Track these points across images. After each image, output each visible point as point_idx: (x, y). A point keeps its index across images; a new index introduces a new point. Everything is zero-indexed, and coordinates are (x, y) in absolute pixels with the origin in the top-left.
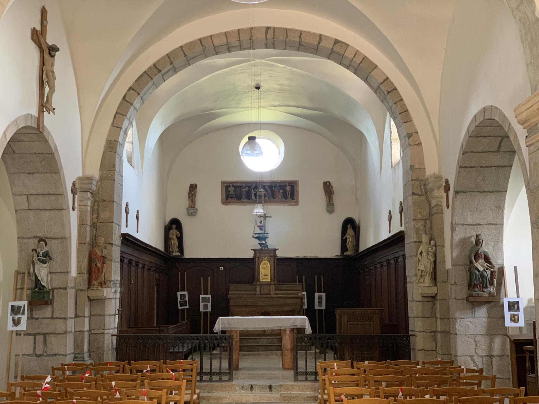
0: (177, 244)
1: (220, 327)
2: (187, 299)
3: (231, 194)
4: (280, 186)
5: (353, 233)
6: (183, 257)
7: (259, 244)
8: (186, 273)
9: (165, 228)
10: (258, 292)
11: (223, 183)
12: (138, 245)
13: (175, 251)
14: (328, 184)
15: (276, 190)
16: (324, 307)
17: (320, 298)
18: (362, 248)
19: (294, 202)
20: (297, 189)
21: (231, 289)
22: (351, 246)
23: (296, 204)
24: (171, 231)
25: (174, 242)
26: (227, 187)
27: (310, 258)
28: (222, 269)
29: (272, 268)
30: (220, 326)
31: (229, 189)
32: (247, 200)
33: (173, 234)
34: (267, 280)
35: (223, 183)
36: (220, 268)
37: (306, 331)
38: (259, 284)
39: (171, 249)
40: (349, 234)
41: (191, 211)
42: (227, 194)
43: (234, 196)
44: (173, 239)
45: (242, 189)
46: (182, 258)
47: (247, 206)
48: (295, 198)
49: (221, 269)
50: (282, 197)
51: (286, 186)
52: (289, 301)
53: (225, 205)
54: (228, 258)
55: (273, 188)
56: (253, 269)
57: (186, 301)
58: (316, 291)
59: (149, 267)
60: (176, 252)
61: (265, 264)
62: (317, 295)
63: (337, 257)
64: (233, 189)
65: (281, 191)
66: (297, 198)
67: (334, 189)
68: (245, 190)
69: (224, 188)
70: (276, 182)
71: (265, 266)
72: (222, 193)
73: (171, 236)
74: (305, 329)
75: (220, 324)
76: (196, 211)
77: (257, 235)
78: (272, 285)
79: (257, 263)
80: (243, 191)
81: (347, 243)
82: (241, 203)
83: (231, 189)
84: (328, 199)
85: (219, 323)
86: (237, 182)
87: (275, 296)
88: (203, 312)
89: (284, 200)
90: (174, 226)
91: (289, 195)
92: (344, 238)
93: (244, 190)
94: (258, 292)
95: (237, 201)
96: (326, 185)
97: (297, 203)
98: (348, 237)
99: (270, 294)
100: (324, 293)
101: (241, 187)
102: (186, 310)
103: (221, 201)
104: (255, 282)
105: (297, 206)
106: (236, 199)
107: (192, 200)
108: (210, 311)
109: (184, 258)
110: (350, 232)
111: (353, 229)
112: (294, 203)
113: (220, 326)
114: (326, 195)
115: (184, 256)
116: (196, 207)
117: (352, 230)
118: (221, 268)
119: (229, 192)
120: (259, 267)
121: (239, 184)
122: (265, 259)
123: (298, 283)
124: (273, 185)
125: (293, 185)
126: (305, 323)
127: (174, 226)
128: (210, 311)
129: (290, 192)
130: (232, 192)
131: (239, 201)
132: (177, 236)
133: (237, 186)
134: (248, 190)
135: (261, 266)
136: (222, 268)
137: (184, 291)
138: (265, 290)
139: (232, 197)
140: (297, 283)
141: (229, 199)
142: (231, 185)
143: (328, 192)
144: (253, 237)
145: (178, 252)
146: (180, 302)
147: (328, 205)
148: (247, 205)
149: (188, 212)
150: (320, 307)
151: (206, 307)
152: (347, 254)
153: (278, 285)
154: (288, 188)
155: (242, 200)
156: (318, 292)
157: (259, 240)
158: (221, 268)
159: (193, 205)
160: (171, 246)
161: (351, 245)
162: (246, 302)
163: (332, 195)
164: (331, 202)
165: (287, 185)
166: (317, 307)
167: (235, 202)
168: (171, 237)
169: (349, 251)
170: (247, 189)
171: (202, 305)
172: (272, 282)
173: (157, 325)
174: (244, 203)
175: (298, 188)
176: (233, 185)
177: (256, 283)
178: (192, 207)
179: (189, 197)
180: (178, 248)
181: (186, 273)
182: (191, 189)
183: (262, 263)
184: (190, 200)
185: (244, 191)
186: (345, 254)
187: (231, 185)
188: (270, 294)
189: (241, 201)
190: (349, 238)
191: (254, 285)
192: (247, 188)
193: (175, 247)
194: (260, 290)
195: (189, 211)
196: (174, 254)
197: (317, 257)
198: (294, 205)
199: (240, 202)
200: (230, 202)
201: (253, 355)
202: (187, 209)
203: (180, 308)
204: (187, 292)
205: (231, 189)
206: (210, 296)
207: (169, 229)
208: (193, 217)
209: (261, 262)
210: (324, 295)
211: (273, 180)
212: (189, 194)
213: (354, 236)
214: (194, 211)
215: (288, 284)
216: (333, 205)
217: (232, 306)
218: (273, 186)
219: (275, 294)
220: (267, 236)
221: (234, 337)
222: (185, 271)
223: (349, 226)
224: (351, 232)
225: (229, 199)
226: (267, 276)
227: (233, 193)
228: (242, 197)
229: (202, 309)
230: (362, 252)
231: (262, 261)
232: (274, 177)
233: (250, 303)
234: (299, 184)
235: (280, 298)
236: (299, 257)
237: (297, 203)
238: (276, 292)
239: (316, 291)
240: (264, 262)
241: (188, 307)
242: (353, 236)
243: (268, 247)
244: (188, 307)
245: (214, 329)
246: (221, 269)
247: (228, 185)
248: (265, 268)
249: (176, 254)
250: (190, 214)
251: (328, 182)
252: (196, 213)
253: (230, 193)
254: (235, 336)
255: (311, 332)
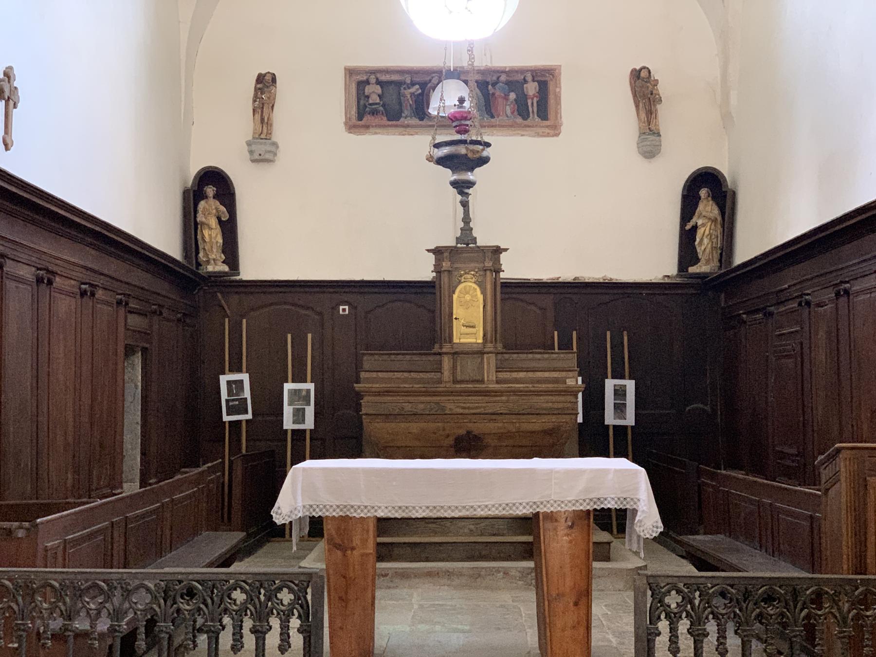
0: (221, 241)
1: (300, 504)
2: (247, 393)
3: (371, 104)
4: (508, 83)
5: (716, 212)
6: (238, 278)
7: (455, 184)
8: (244, 321)
9: (186, 193)
10: (447, 374)
11: (350, 72)
12: (78, 226)
13: (214, 260)
14: (644, 74)
15: (498, 93)
16: (630, 420)
17: (620, 393)
18: (744, 253)
19: (547, 127)
20: (558, 90)
21: (366, 366)
22: (708, 250)
23: (552, 132)
24: (202, 204)
25: (210, 235)
26: (361, 85)
27: (590, 281)
28: (347, 312)
29: (489, 308)
30: (299, 498)
31: (368, 90)
32: (415, 121)
33: (206, 213)
34: (473, 341)
35: (350, 72)
36: (341, 307)
37: (640, 521)
38: (448, 351)
39: (201, 255)
40: (704, 213)
41: (260, 148)
42: (362, 102)
43: (381, 108)
44: (208, 225)
45: (402, 91)
46: (237, 281)
47: (416, 137)
48: (551, 115)
49: (344, 310)
50: (512, 113)
51: (525, 81)
52: (542, 402)
53: (354, 133)
54: (362, 281)
55: (490, 87)
56: (433, 312)
57: (289, 405)
58: (609, 375)
59: (83, 286)
60: (216, 264)
61: (467, 293)
62: (610, 384)
63: (667, 280)
64: (378, 89)
65: (512, 96)
66: (556, 117)
67: (663, 89)
68: (412, 94)
69: (354, 86)
70: (498, 72)
71: (468, 297)
72: (347, 100)
73: (200, 218)
74: (635, 512)
75: (299, 492)
76: (273, 149)
77: (445, 151)
78: (488, 353)
79: (445, 292)
80: (404, 96)
81: (698, 240)
82: (401, 129)
83: (373, 90)
84: (643, 115)
85: (294, 483)
86: (387, 71)
87: (497, 387)
88: (293, 431)
89: (519, 120)
90: (210, 191)
91: (533, 107)
92: (688, 227)
93: (408, 92)
94: (447, 374)
95: (390, 123)
96: (638, 77)
97: (555, 130)
98: (700, 222)
99: (482, 381)
100: (630, 379)
101: (399, 84)
102: (244, 425)
103: (346, 124)
104: (437, 346)
105: (555, 138)
106: (385, 118)
107: (262, 120)
108: (313, 427)
109: (241, 281)
110: (707, 208)
111: (714, 198)
112: (547, 130)
113: (299, 498)
114: (637, 106)
115: (238, 274)
116: (275, 138)
117: (711, 202)
118: (344, 309)
119: (368, 97)
120: (451, 302)
121: (395, 78)
122: (469, 276)
123: (559, 349)
124: (489, 79)
125: (543, 79)
126: (637, 489)
127: (210, 191)
128: (313, 427)
129: (535, 100)
130: (374, 99)
131: (394, 123)
132: (219, 219)
133: (390, 83)
134: (420, 91)
135: (455, 297)
136: (347, 307)
137: (240, 371)
138: (468, 367)
139: (374, 113)
140: (557, 350)
141: (365, 119)
142: (373, 80)
143: (644, 96)
144: (430, 159)
145: (223, 262)
146: (227, 401)
147: (642, 133)
148: (417, 133)
149: (251, 152)
150: (620, 418)
151: (299, 416)
152: (698, 271)
153: (507, 356)
154: (531, 88)
155: (402, 119)
156: (613, 378)
157: (454, 169)
158: (344, 309)
159: (265, 131)
160: (201, 247)
161: (709, 246)
162: (410, 405)
163: (655, 105)
164: (652, 127)
165: (529, 77)
166: (610, 419)
167: (384, 126)
168: (204, 220)
169: (703, 261)
170: (416, 89)
171: (288, 411)
172: (489, 345)
173: (246, 451)
174: (408, 130)
175: (560, 88)
176: (377, 79)
177: (441, 348)
178: (263, 136)
179: (254, 111)
180: (223, 252)
181: (244, 321)
182: (259, 86)
183: (458, 290)
184: (258, 117)
185: (409, 96)
186: (692, 270)
187: (373, 80)
188: (482, 381)
189: (398, 123)
190: (703, 225)
191: (435, 354)
192: (417, 86)
193: (215, 250)
194: (454, 368)
195: (254, 147)
196: (210, 268)
197: (611, 279)
198: (548, 135)
199: (396, 126)
200: (367, 127)
201: (430, 574)
202: (249, 144)
203: (226, 418)
204: (248, 375)
205: (373, 90)
206: (311, 386)
207: (194, 196)
208: (266, 165)
209: (456, 287)
210: (630, 385)
211: (489, 65)
212: (254, 101)
213: (719, 219)
214: (269, 148)
215: (536, 353)
216: (659, 135)
217: (366, 414)
218: (487, 83)
219: (498, 382)
220: (485, 154)
221: (356, 541)
222: (243, 316)
223: (703, 192)
224: (709, 208)
225: (368, 119)
226: (473, 327)
227: (378, 101)
228: (401, 111)
229: (288, 424)
230: (739, 266)
231: (460, 282)
232: (491, 57)
233: (421, 406)
234: (562, 75)
235: (515, 392)
236: (560, 280)
237: (555, 130)
238: (502, 375)
239: (609, 375)
240: (465, 287)
241: (249, 416)
242: (714, 221)
243: (476, 243)
244: (249, 416)
245: (275, 509)
246: (344, 310)
247: (365, 78)
248: (466, 305)
249: (216, 266)
250: (256, 157)
251: (644, 68)
252: (275, 154)
253: (371, 101)
254: (358, 537)
255: (660, 524)
